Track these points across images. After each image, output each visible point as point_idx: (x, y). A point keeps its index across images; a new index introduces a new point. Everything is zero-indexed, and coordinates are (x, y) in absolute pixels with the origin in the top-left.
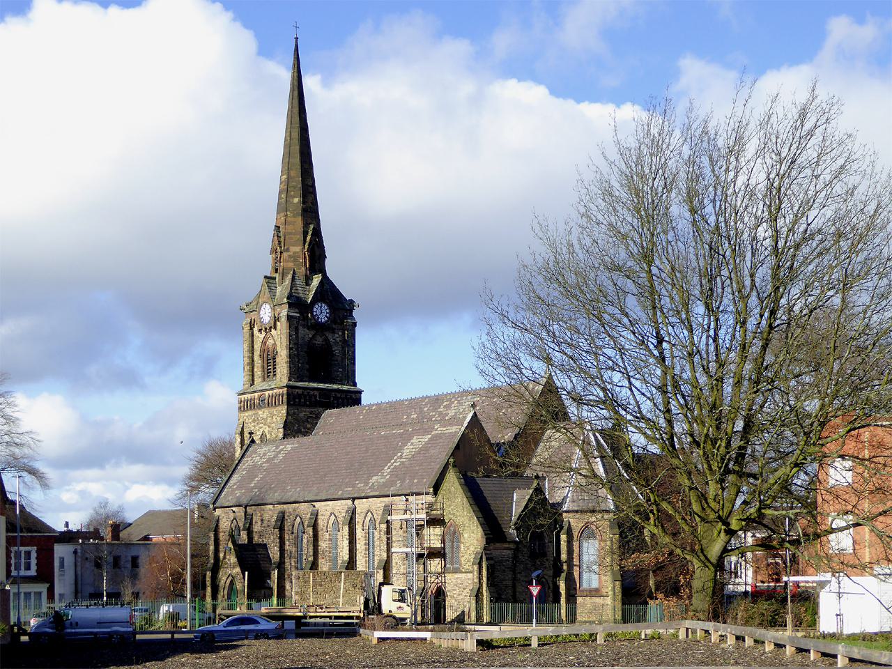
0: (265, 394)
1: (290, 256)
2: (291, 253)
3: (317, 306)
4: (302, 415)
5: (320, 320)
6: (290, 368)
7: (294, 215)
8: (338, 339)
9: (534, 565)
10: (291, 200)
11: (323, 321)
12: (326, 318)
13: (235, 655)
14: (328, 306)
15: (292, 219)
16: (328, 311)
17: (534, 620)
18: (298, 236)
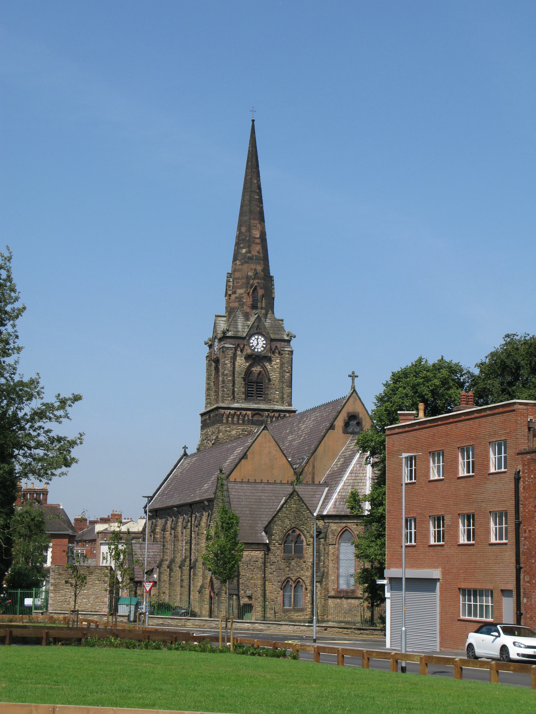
0: (426, 415)
1: (236, 298)
2: (237, 295)
3: (253, 338)
4: (234, 432)
5: (256, 350)
6: (394, 391)
7: (242, 262)
8: (275, 366)
9: (289, 567)
10: (240, 251)
11: (259, 350)
12: (262, 349)
13: (26, 622)
14: (264, 338)
15: (240, 267)
16: (264, 342)
17: (19, 596)
18: (244, 281)
